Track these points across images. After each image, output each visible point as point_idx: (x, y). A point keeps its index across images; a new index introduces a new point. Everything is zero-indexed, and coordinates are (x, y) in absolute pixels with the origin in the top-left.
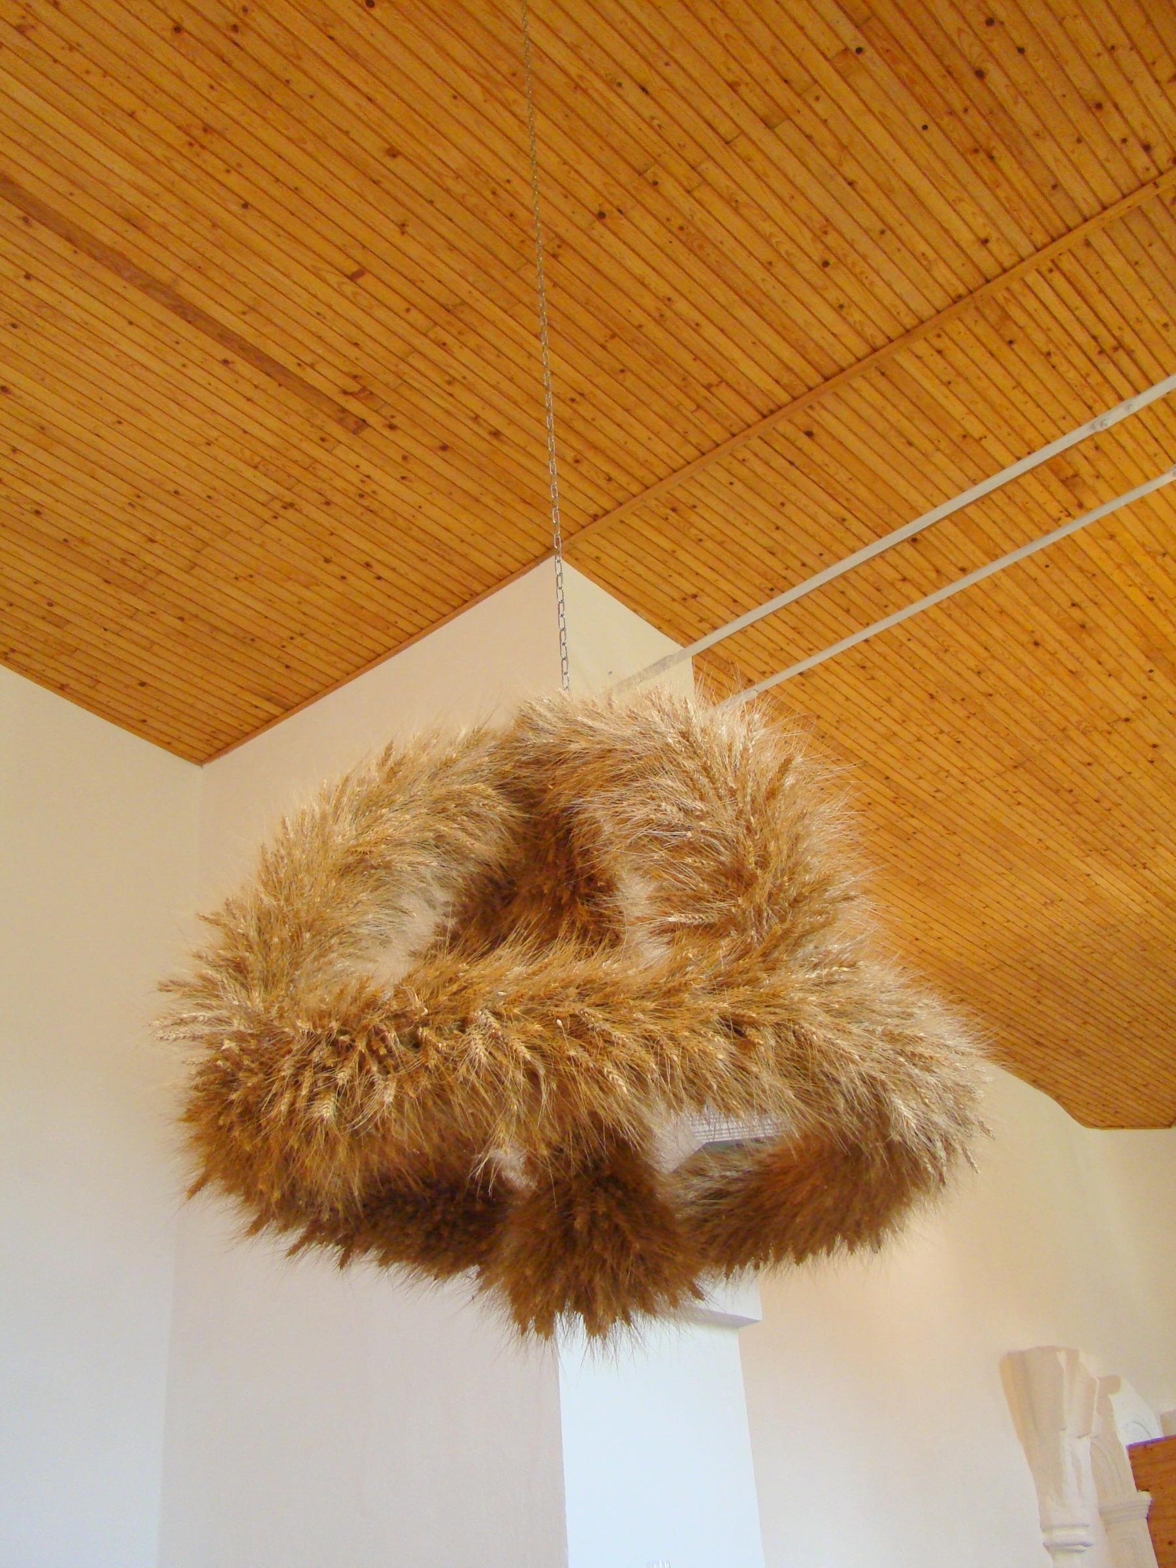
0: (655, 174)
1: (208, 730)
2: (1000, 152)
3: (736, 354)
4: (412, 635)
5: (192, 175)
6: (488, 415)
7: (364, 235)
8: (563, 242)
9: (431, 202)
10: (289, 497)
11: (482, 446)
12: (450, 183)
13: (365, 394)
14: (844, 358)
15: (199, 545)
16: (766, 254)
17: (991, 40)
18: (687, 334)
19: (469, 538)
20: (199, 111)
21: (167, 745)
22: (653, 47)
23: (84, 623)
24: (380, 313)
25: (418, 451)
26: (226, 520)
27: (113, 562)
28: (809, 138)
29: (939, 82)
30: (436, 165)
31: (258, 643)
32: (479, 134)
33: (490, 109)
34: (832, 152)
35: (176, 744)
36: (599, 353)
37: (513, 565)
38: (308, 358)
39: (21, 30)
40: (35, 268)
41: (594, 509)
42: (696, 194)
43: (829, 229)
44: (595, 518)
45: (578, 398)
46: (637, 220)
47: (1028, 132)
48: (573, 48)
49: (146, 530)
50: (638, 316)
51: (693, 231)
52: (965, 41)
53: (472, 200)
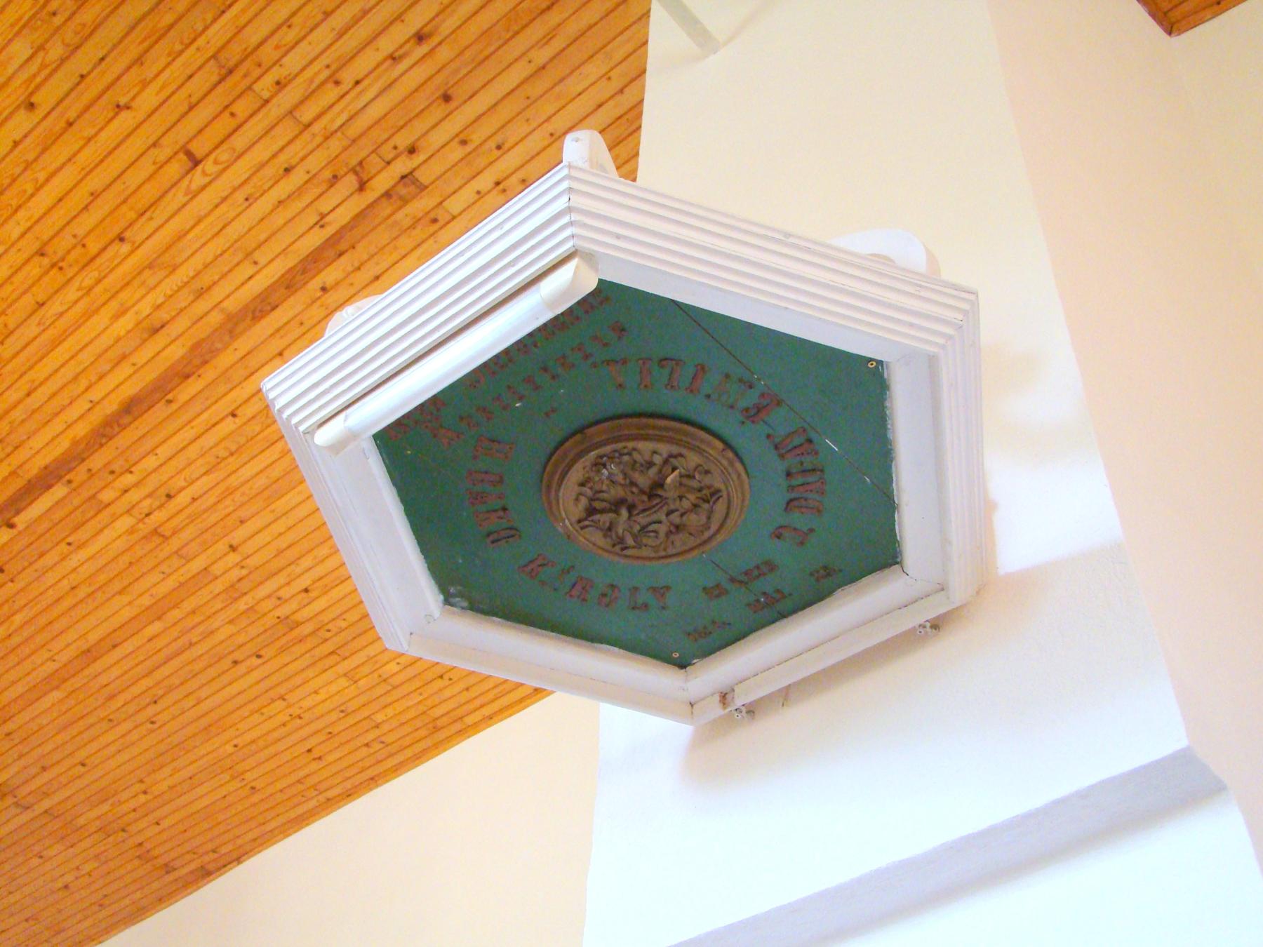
6: (386, 45)
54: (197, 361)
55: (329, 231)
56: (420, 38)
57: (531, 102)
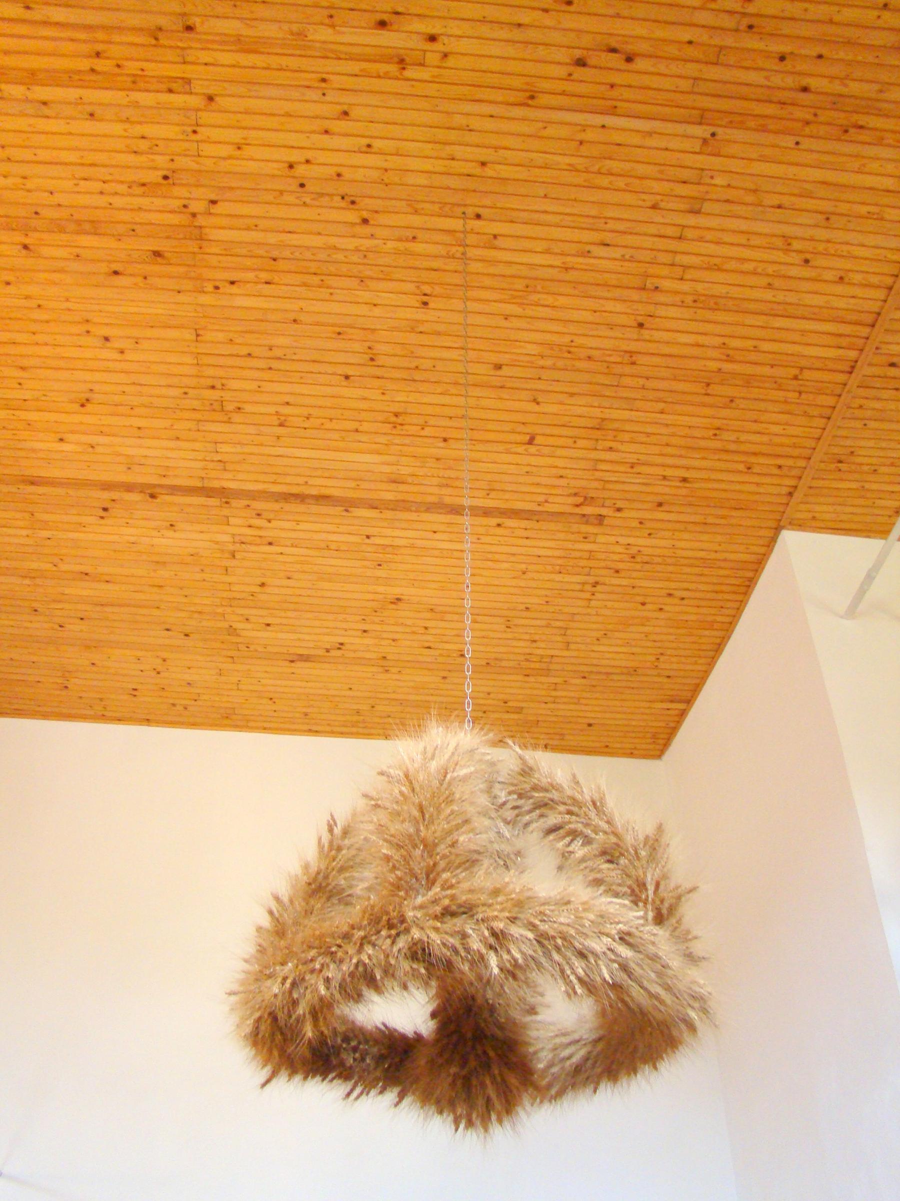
0: (652, 283)
1: (649, 735)
2: (862, 120)
3: (797, 349)
4: (731, 623)
5: (407, 441)
6: (669, 472)
7: (519, 417)
8: (631, 353)
9: (540, 379)
10: (591, 579)
11: (683, 492)
12: (542, 363)
13: (588, 500)
14: (875, 307)
15: (563, 632)
16: (764, 281)
17: (794, 67)
18: (753, 357)
19: (719, 548)
20: (386, 409)
21: (631, 755)
22: (591, 220)
23: (532, 705)
24: (559, 452)
25: (648, 515)
26: (566, 610)
27: (522, 663)
28: (727, 201)
29: (783, 113)
30: (527, 358)
31: (640, 671)
32: (533, 328)
33: (529, 312)
34: (750, 198)
35: (636, 752)
36: (707, 399)
37: (763, 550)
38: (541, 498)
39: (281, 425)
40: (370, 531)
41: (785, 490)
42: (686, 277)
43: (790, 241)
44: (790, 494)
45: (717, 432)
46: (663, 314)
47: (873, 96)
48: (547, 252)
49: (527, 637)
50: (713, 365)
51: (703, 298)
52: (777, 80)
53: (560, 364)
54: (391, 506)
55: (540, 509)
56: (685, 480)
57: (686, 530)
